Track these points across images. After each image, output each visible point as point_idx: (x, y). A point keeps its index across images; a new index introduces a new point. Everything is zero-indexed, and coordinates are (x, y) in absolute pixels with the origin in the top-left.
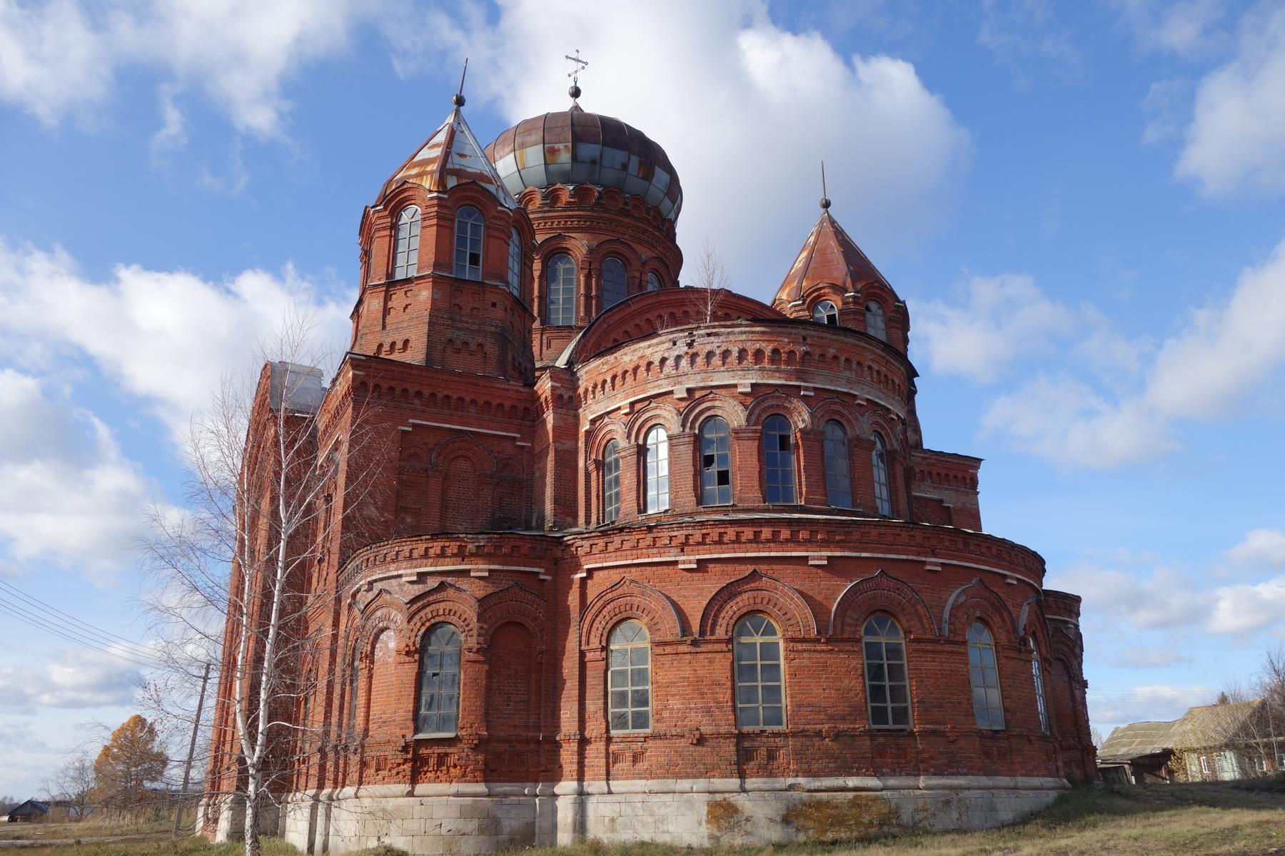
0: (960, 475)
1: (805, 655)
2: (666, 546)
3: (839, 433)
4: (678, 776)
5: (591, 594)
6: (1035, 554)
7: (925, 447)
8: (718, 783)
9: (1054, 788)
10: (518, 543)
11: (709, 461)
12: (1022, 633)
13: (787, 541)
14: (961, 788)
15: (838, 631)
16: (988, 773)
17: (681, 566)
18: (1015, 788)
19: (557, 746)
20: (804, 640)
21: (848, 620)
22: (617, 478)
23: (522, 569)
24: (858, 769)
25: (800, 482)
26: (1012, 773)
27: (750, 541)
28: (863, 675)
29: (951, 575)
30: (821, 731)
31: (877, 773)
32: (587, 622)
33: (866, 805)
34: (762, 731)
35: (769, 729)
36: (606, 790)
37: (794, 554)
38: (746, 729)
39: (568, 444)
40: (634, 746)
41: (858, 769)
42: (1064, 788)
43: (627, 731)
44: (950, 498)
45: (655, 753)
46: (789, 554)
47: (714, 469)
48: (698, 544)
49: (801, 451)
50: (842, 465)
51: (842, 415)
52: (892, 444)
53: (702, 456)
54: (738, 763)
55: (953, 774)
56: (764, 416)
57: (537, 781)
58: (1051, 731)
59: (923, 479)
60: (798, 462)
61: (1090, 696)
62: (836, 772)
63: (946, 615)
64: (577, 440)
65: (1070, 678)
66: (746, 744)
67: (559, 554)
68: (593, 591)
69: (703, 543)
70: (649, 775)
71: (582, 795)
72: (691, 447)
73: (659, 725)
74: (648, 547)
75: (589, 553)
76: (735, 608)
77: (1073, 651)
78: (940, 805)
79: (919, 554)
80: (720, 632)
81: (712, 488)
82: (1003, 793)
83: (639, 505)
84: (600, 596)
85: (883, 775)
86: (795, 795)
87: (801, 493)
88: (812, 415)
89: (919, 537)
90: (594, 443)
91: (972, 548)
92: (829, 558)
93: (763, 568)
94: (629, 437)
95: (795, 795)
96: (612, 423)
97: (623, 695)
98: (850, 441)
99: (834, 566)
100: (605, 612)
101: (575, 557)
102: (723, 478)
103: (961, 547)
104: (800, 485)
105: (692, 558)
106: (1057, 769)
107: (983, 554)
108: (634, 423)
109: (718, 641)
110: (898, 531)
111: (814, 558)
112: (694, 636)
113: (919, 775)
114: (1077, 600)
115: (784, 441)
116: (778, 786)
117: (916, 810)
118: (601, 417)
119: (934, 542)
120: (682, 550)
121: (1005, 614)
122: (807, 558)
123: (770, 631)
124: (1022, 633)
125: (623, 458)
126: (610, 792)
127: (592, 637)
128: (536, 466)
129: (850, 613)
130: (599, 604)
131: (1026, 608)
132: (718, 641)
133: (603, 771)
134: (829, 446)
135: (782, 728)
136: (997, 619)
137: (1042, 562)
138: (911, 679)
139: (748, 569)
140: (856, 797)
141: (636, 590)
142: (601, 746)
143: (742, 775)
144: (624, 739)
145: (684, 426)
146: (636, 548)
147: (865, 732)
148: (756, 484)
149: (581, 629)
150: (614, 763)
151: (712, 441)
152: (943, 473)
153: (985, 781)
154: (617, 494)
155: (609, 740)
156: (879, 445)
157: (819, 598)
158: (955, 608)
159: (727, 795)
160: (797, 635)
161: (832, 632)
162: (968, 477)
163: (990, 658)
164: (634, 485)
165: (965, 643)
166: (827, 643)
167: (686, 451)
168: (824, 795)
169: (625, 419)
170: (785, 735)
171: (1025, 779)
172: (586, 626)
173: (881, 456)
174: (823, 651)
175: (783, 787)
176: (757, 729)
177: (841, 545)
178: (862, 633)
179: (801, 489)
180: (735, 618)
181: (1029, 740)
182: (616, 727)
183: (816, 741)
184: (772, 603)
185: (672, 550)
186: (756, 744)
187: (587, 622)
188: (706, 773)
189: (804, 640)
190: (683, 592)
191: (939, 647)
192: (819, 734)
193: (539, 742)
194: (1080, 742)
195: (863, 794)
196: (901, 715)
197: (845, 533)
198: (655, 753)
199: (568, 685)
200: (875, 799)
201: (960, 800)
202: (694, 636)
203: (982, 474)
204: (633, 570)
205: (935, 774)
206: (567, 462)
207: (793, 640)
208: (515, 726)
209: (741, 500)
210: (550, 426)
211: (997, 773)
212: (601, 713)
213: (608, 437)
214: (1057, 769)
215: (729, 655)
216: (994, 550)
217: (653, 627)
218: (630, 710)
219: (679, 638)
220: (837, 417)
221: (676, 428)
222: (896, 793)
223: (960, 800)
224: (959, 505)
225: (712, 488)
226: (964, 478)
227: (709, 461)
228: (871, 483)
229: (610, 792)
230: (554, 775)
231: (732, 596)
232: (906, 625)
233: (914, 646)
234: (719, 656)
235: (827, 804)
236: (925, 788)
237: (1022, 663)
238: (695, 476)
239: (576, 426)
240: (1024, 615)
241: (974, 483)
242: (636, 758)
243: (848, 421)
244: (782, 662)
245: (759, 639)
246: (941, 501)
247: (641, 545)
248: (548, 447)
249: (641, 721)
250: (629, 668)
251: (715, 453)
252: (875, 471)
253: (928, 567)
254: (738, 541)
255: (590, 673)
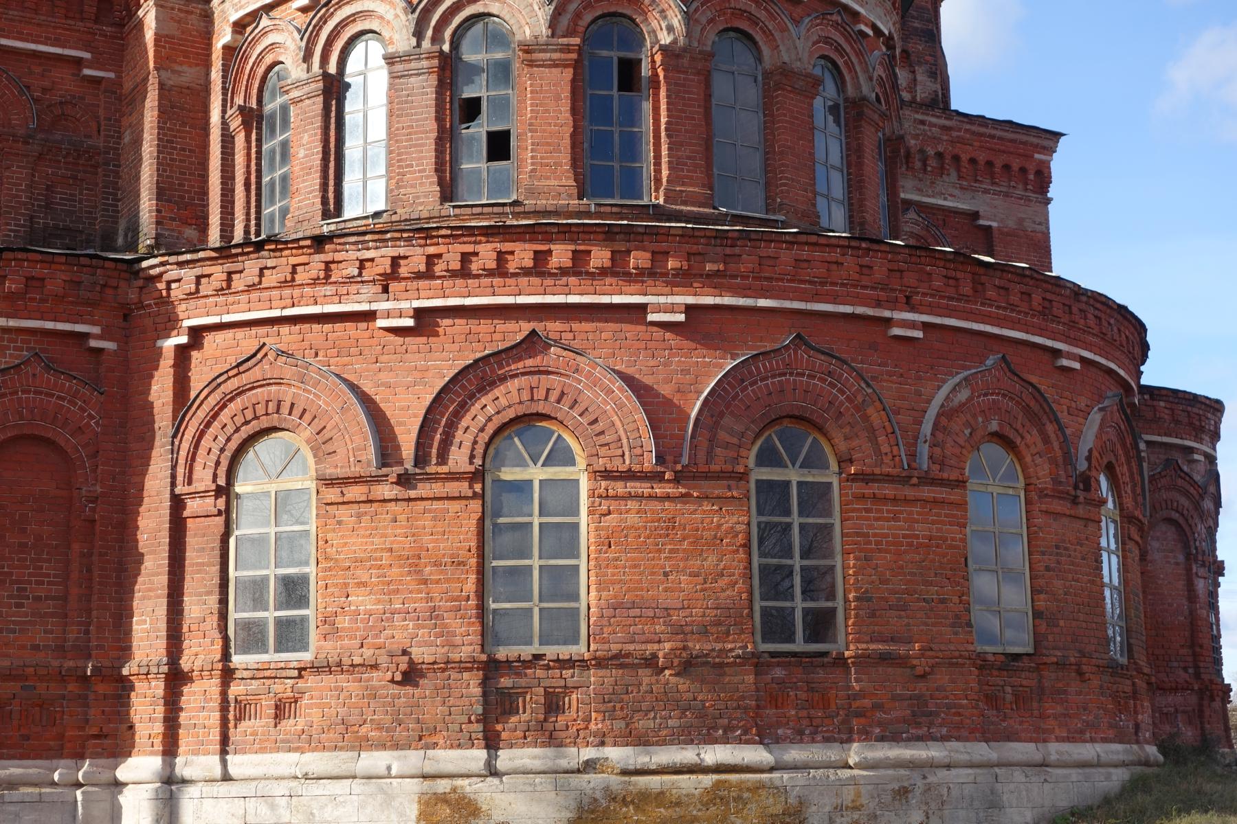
0: (1016, 164)
1: (632, 505)
2: (350, 280)
3: (744, 57)
4: (362, 744)
5: (199, 377)
6: (1123, 310)
7: (954, 106)
8: (448, 758)
9: (1123, 764)
10: (38, 270)
11: (471, 109)
12: (1082, 466)
13: (603, 272)
14: (932, 765)
15: (701, 456)
16: (988, 735)
17: (381, 323)
18: (1044, 764)
19: (124, 687)
20: (629, 475)
21: (722, 435)
22: (285, 145)
23: (50, 325)
24: (727, 729)
25: (658, 157)
26: (1040, 736)
27: (526, 272)
28: (747, 546)
29: (942, 347)
30: (655, 656)
31: (765, 737)
32: (189, 436)
33: (738, 799)
34: (537, 657)
35: (551, 651)
36: (218, 772)
37: (617, 299)
38: (502, 653)
39: (188, 74)
40: (277, 687)
41: (727, 729)
42: (1147, 763)
43: (264, 657)
44: (992, 210)
45: (321, 700)
46: (605, 299)
47: (479, 130)
48: (419, 276)
49: (663, 93)
50: (749, 125)
51: (754, 21)
52: (858, 86)
53: (455, 105)
54: (485, 719)
55: (919, 739)
56: (588, 18)
57: (80, 756)
58: (1131, 656)
59: (941, 171)
60: (655, 115)
61: (1220, 590)
62: (686, 737)
63: (927, 428)
64: (208, 65)
65: (1188, 556)
66: (505, 682)
67: (133, 296)
68: (201, 372)
69: (428, 274)
70: (306, 742)
71: (171, 784)
72: (433, 80)
73: (329, 644)
74: (315, 282)
75: (194, 294)
76: (490, 410)
77: (1197, 506)
78: (887, 798)
79: (878, 304)
80: (459, 459)
81: (475, 163)
82: (1018, 775)
83: (325, 201)
84: (214, 384)
85: (778, 740)
86: (593, 781)
87: (658, 181)
88: (688, 18)
89: (880, 268)
90: (240, 71)
91: (991, 293)
92: (689, 309)
93: (553, 328)
94: (307, 57)
95: (593, 781)
96: (276, 29)
97: (258, 586)
98: (767, 75)
99: (698, 326)
100: (225, 416)
101: (165, 302)
102: (499, 146)
103: (966, 289)
104: (658, 164)
105: (405, 305)
106: (1137, 727)
107: (1012, 307)
108: (318, 28)
109: (453, 477)
110: (836, 255)
111: (659, 309)
112: (404, 463)
113: (850, 740)
114: (1215, 408)
115: (628, 74)
116: (563, 764)
117: (839, 808)
118: (254, 16)
119: (911, 279)
120: (386, 290)
121: (1050, 428)
122: (643, 308)
123: (561, 456)
124: (1082, 466)
125: (296, 101)
126: (226, 777)
127: (198, 467)
128: (125, 122)
129: (727, 420)
130: (212, 400)
131: (1096, 417)
132: (453, 477)
133: (215, 735)
134: (721, 87)
135: (579, 650)
136: (1033, 437)
137: (1141, 328)
138: (846, 553)
139: (518, 330)
140: (717, 785)
141: (288, 372)
142: (212, 686)
143: (492, 743)
144: (259, 673)
145: (418, 34)
146: (289, 283)
147: (744, 659)
148: (565, 158)
149: (174, 451)
150: (238, 719)
151: (475, 69)
152: (982, 157)
153: (981, 751)
154: (284, 179)
155: (228, 674)
156: (830, 89)
157: (665, 390)
158: (947, 413)
159: (459, 782)
160: (618, 465)
161: (686, 457)
162: (1032, 169)
163: (1014, 514)
164: (317, 160)
165: (961, 483)
166: (677, 480)
167: (424, 88)
168: (654, 782)
169: (301, 20)
170: (583, 664)
171: (1066, 747)
172: (185, 446)
173: (834, 110)
174: (668, 497)
175: (574, 765)
176: (527, 652)
177: (715, 282)
178: (751, 462)
179: (658, 171)
180: (490, 430)
181: (1080, 673)
182: (246, 650)
183: (646, 676)
184: (567, 400)
185: (365, 289)
186: (522, 682)
187: (189, 436)
188: (423, 739)
189: (629, 475)
190: (384, 377)
191: (909, 492)
192: (650, 662)
193: (84, 679)
194: (1197, 675)
195: (733, 777)
196: (820, 625)
197: (726, 259)
198: (321, 700)
199: (149, 564)
200: (758, 787)
201: (928, 788)
202: (404, 463)
203: (1060, 164)
204: (285, 329)
205: (882, 739)
206: (184, 112)
207: (607, 475)
208: (36, 648)
209: (531, 192)
210: (149, 35)
211: (1010, 737)
212: (213, 621)
213: (269, 59)
214: (1137, 727)
215: (476, 505)
216: (1037, 298)
217: (322, 447)
218: (270, 615)
219: (373, 470)
220: (744, 25)
221: (402, 40)
222: (800, 777)
223: (928, 788)
224: (1011, 224)
225: (475, 163)
226: (1023, 170)
227: (471, 109)
228: (809, 163)
229: (226, 777)
230: (115, 742)
231: (486, 385)
232: (843, 446)
233: (857, 488)
234: (455, 506)
235: (660, 797)
236: (858, 766)
237: (1078, 525)
238: (439, 141)
239: (207, 36)
240: (1089, 433)
241: (1042, 180)
242: (281, 711)
243: (767, 33)
244: (584, 518)
245: (537, 473)
246: (975, 215)
247: (301, 277)
248: (146, 79)
249: (291, 634)
250: (272, 530)
251: (483, 94)
252: (819, 139)
253: (897, 331)
254: (500, 270)
255: (193, 542)
